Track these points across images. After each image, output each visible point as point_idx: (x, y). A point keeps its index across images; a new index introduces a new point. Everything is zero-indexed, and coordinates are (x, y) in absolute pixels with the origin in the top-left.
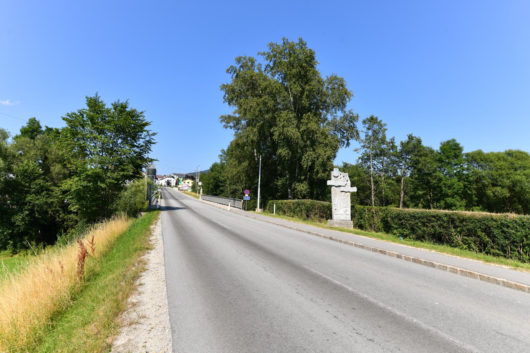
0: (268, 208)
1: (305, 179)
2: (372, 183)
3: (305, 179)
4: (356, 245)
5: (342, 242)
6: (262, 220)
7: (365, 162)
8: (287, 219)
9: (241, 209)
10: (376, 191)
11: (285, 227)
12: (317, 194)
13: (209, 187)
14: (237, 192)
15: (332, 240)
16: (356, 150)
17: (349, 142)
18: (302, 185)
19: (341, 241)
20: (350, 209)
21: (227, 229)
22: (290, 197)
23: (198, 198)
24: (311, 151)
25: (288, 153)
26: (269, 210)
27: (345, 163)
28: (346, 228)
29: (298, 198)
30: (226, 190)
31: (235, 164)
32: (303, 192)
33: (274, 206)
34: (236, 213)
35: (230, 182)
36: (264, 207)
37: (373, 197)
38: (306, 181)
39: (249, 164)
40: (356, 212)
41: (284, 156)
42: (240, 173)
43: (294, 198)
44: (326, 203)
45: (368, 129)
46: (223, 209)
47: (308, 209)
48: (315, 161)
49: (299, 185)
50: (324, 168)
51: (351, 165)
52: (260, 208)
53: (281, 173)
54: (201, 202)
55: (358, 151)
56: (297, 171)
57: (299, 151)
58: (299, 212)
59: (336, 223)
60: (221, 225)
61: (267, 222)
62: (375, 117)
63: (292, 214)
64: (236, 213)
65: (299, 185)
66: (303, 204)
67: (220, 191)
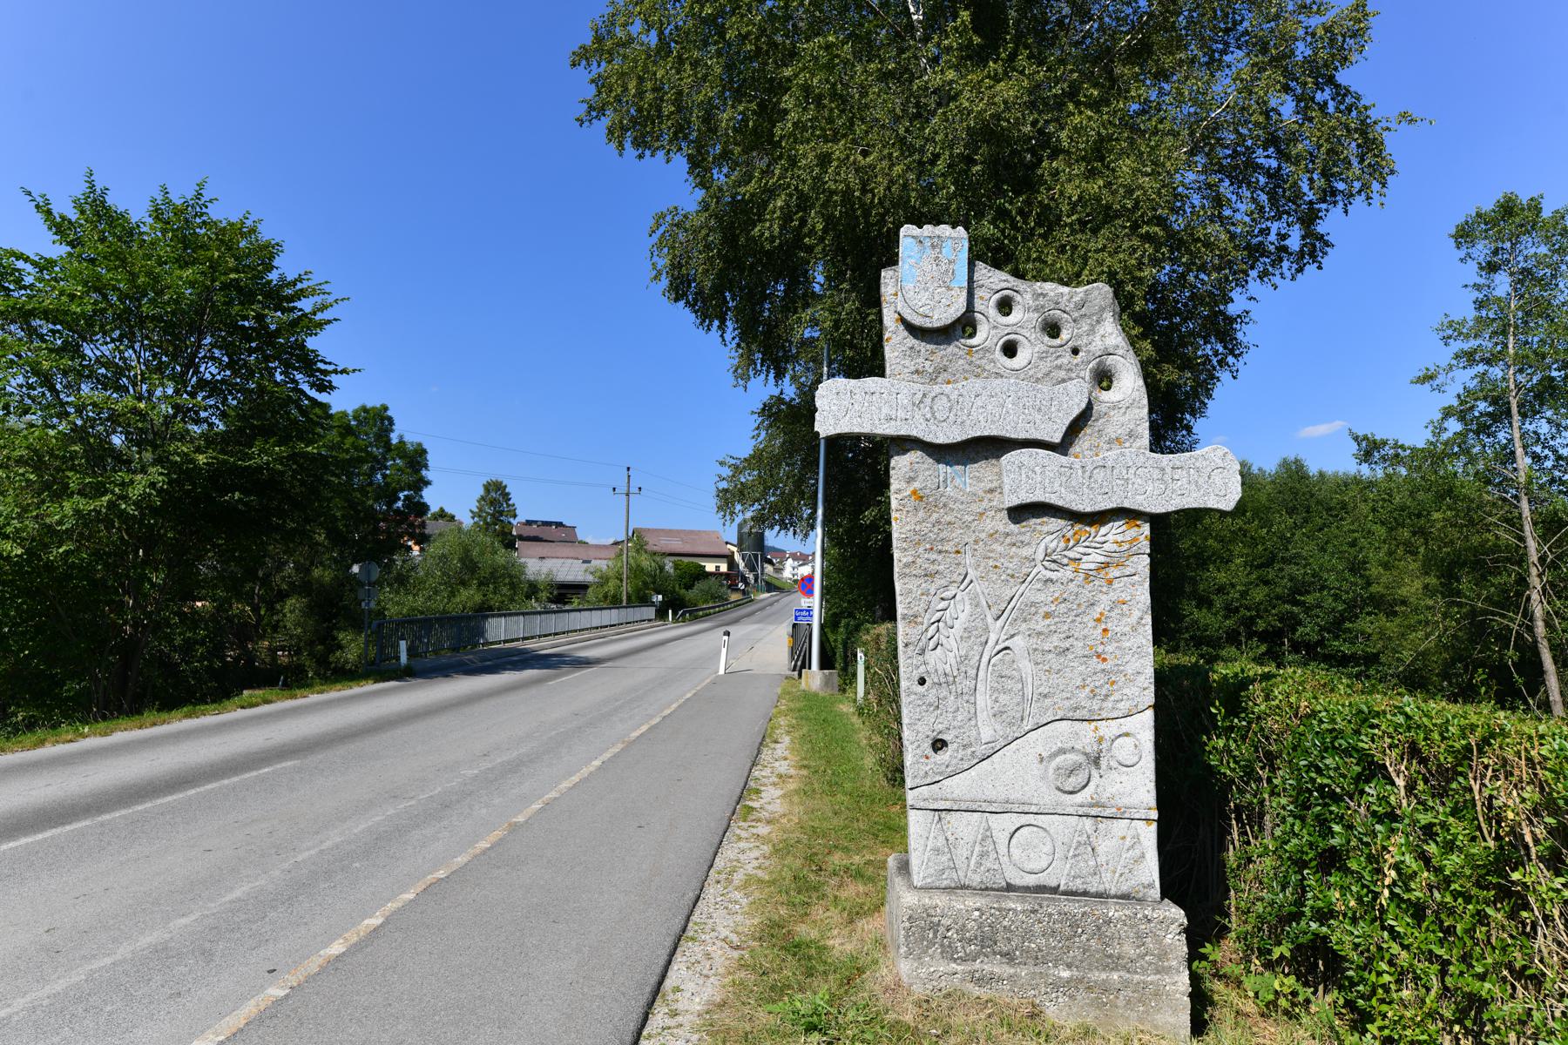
2: (1528, 528)
7: (1483, 429)
10: (1554, 566)
16: (1428, 378)
17: (1321, 228)
27: (1366, 438)
37: (1535, 596)
45: (1492, 268)
51: (1402, 447)
55: (1437, 382)
62: (1524, 199)
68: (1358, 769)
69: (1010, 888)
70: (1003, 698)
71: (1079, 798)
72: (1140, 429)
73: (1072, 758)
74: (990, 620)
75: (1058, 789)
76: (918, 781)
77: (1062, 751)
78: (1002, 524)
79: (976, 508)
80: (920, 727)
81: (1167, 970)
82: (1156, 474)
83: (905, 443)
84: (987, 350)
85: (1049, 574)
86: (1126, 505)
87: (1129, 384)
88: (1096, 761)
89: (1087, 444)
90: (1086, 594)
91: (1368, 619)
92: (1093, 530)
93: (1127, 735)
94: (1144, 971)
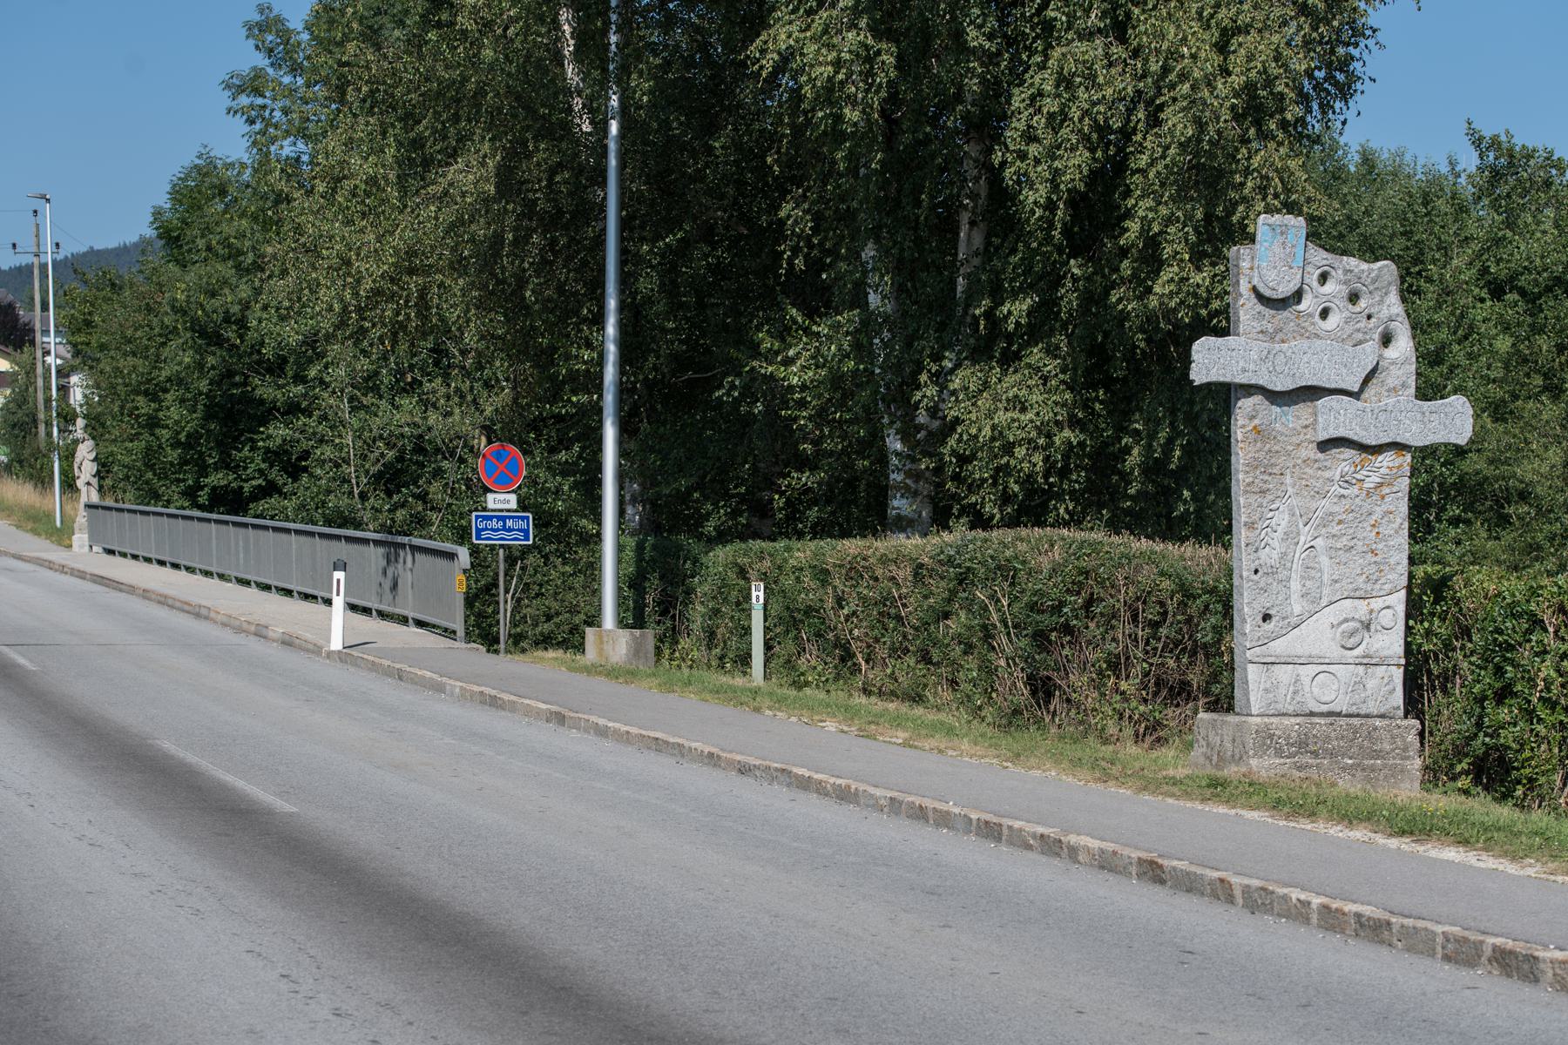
0: (696, 626)
1: (1038, 328)
3: (1038, 328)
4: (1331, 920)
5: (1230, 899)
6: (625, 738)
8: (850, 713)
9: (449, 633)
11: (805, 784)
12: (1153, 468)
13: (153, 423)
14: (438, 473)
15: (1162, 882)
18: (1010, 384)
19: (1222, 892)
20: (1401, 609)
21: (269, 812)
22: (900, 505)
23: (62, 535)
24: (1088, 35)
25: (868, 58)
26: (711, 635)
27: (1495, 143)
28: (1347, 785)
29: (980, 521)
30: (328, 452)
31: (372, 181)
32: (1020, 452)
33: (748, 597)
34: (401, 676)
35: (364, 364)
36: (666, 607)
38: (1052, 352)
39: (507, 182)
40: (1466, 633)
41: (830, 93)
42: (426, 271)
43: (941, 519)
44: (1191, 556)
46: (288, 642)
47: (1046, 620)
48: (1126, 133)
49: (986, 385)
50: (1210, 205)
52: (622, 623)
53: (815, 266)
54: (82, 575)
56: (968, 240)
57: (974, 38)
58: (969, 649)
59: (1267, 740)
60: (224, 787)
61: (659, 746)
63: (907, 669)
64: (401, 676)
65: (986, 385)
66: (1006, 571)
67: (273, 456)
68: (1526, 626)
69: (1312, 714)
70: (1308, 583)
71: (1356, 652)
72: (1409, 381)
73: (1352, 625)
74: (1301, 526)
75: (1343, 647)
76: (1254, 644)
77: (1346, 620)
78: (1311, 452)
79: (1295, 440)
80: (1255, 604)
81: (1407, 758)
82: (1419, 416)
83: (1250, 390)
84: (1310, 315)
85: (1343, 491)
86: (1398, 440)
87: (1403, 345)
88: (1367, 627)
89: (1373, 392)
90: (1367, 507)
91: (1453, 532)
92: (1373, 458)
93: (1388, 607)
94: (1394, 758)
